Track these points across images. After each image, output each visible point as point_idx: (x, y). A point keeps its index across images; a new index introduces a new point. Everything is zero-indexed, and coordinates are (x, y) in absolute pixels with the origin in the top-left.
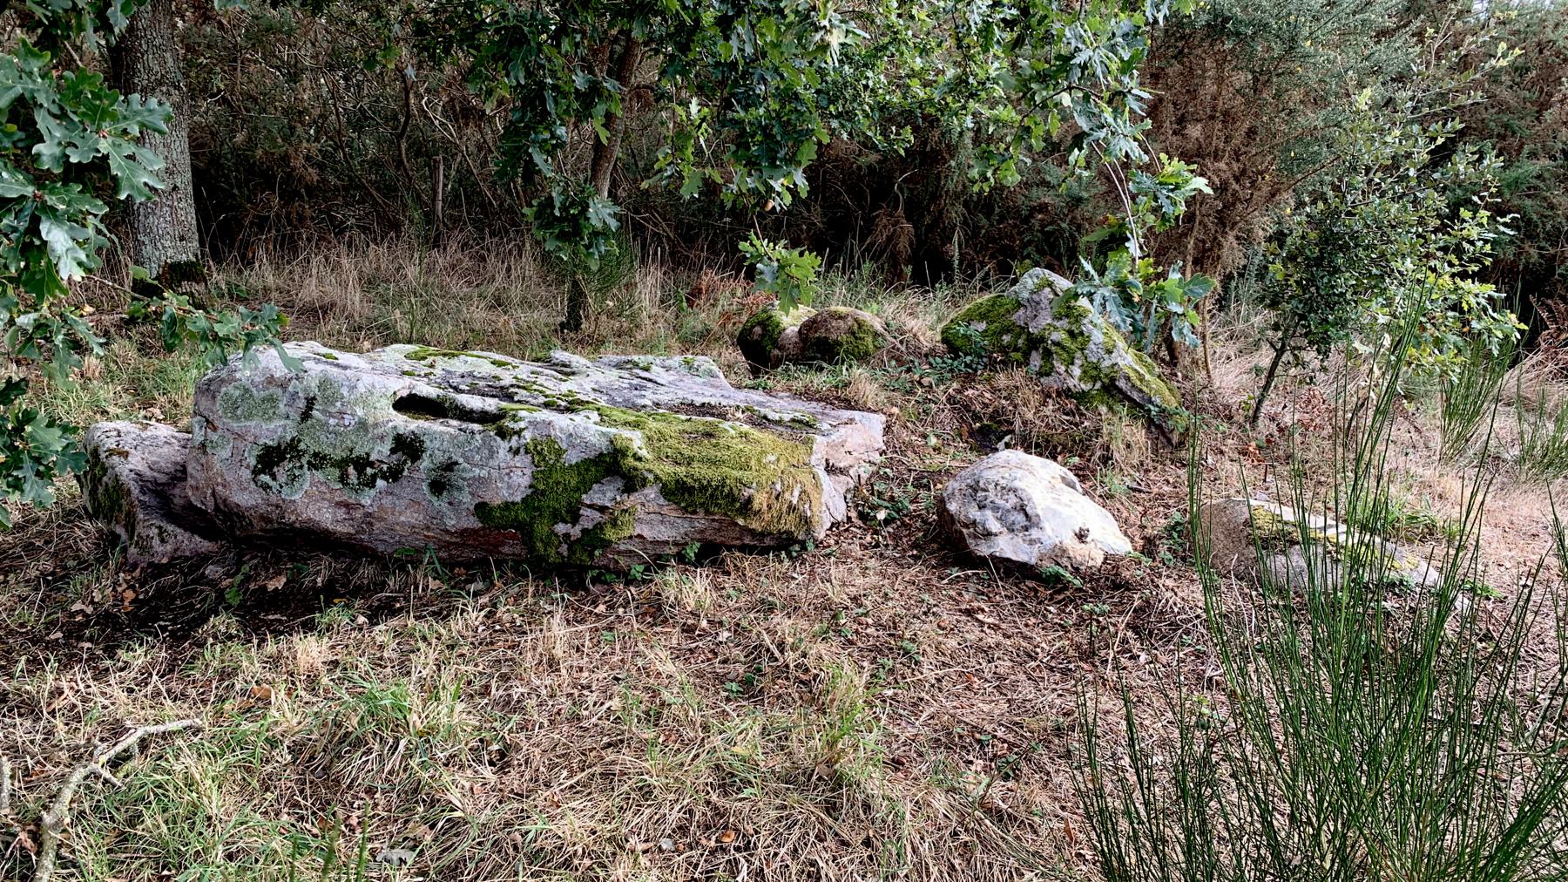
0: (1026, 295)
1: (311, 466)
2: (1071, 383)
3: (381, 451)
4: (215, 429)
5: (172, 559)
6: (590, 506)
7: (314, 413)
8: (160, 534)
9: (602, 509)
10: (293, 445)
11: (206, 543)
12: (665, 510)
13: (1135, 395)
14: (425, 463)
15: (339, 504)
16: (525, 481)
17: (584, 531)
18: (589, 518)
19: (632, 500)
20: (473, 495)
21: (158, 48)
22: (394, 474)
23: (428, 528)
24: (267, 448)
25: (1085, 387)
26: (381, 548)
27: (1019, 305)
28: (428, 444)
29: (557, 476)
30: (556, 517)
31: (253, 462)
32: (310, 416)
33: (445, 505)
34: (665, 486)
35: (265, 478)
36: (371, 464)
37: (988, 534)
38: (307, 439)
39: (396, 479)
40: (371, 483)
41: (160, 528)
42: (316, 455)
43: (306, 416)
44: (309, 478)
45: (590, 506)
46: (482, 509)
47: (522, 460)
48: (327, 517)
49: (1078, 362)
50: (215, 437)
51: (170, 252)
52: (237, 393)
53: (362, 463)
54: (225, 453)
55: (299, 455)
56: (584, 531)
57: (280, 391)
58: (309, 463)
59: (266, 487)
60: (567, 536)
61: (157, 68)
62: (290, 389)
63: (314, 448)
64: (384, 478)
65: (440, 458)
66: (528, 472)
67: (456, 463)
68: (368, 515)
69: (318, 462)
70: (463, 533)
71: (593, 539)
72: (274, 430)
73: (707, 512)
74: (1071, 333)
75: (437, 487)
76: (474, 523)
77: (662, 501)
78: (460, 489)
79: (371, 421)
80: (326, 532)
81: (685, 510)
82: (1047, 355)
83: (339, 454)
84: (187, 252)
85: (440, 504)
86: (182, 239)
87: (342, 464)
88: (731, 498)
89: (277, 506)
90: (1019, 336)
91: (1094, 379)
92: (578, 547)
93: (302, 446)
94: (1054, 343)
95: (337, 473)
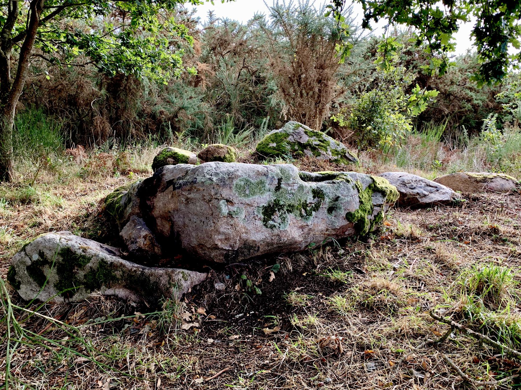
0: (291, 131)
1: (289, 211)
2: (330, 157)
3: (310, 199)
7: (282, 186)
13: (350, 158)
20: (345, 210)
25: (336, 157)
27: (288, 135)
31: (262, 217)
35: (271, 222)
37: (425, 196)
49: (329, 150)
55: (281, 207)
59: (272, 227)
63: (288, 203)
65: (331, 196)
67: (339, 197)
69: (291, 209)
72: (265, 198)
85: (332, 217)
91: (337, 154)
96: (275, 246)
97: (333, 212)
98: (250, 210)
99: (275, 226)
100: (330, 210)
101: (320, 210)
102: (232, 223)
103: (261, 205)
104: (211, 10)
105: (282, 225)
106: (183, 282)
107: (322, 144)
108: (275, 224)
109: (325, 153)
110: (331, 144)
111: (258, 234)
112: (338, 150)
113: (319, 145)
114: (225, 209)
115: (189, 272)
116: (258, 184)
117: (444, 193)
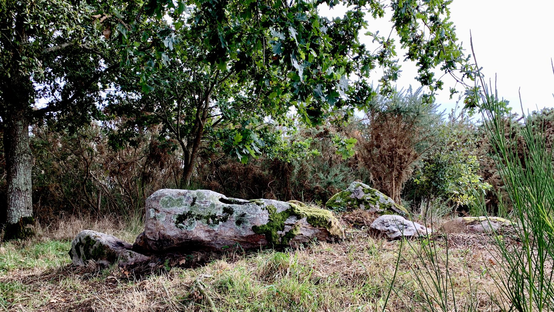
0: (353, 189)
2: (377, 210)
3: (220, 213)
4: (158, 212)
5: (135, 263)
6: (287, 225)
7: (196, 202)
8: (130, 255)
9: (292, 225)
10: (189, 214)
11: (146, 257)
12: (307, 226)
13: (397, 211)
14: (235, 215)
15: (207, 231)
16: (267, 218)
17: (286, 233)
18: (288, 228)
19: (300, 222)
20: (251, 224)
21: (24, 141)
22: (224, 220)
23: (236, 237)
24: (179, 215)
25: (382, 210)
26: (217, 247)
28: (234, 209)
29: (276, 216)
30: (278, 229)
31: (176, 220)
32: (195, 204)
33: (241, 229)
34: (308, 217)
35: (181, 225)
36: (216, 217)
38: (195, 211)
39: (225, 221)
40: (218, 223)
41: (130, 252)
42: (198, 215)
43: (193, 204)
44: (197, 223)
45: (287, 225)
46: (255, 228)
47: (266, 212)
48: (203, 235)
49: (378, 204)
50: (159, 214)
51: (23, 213)
52: (167, 199)
53: (214, 217)
54: (164, 219)
56: (286, 233)
57: (183, 197)
58: (196, 218)
59: (181, 228)
60: (281, 235)
61: (23, 147)
62: (187, 196)
63: (197, 213)
64: (222, 221)
65: (239, 213)
66: (267, 215)
68: (217, 234)
69: (199, 217)
70: (248, 237)
71: (290, 235)
73: (320, 226)
74: (373, 197)
75: (239, 223)
76: (252, 233)
77: (307, 223)
78: (247, 222)
79: (215, 204)
80: (202, 241)
81: (313, 226)
82: (366, 203)
83: (206, 215)
84: (29, 214)
85: (240, 228)
86: (28, 208)
87: (207, 218)
88: (326, 221)
89: (185, 234)
90: (354, 201)
91: (384, 208)
92: (285, 238)
93: (193, 213)
94: (368, 200)
95: (206, 221)
96: (184, 241)
97: (241, 224)
98: (169, 216)
99: (183, 227)
100: (239, 223)
101: (228, 222)
102: (155, 222)
103: (177, 214)
104: (442, 86)
105: (188, 227)
106: (129, 257)
107: (373, 199)
108: (183, 226)
109: (373, 206)
110: (380, 199)
111: (172, 232)
112: (386, 204)
113: (370, 200)
114: (152, 215)
115: (136, 253)
116: (177, 200)
117: (410, 230)
